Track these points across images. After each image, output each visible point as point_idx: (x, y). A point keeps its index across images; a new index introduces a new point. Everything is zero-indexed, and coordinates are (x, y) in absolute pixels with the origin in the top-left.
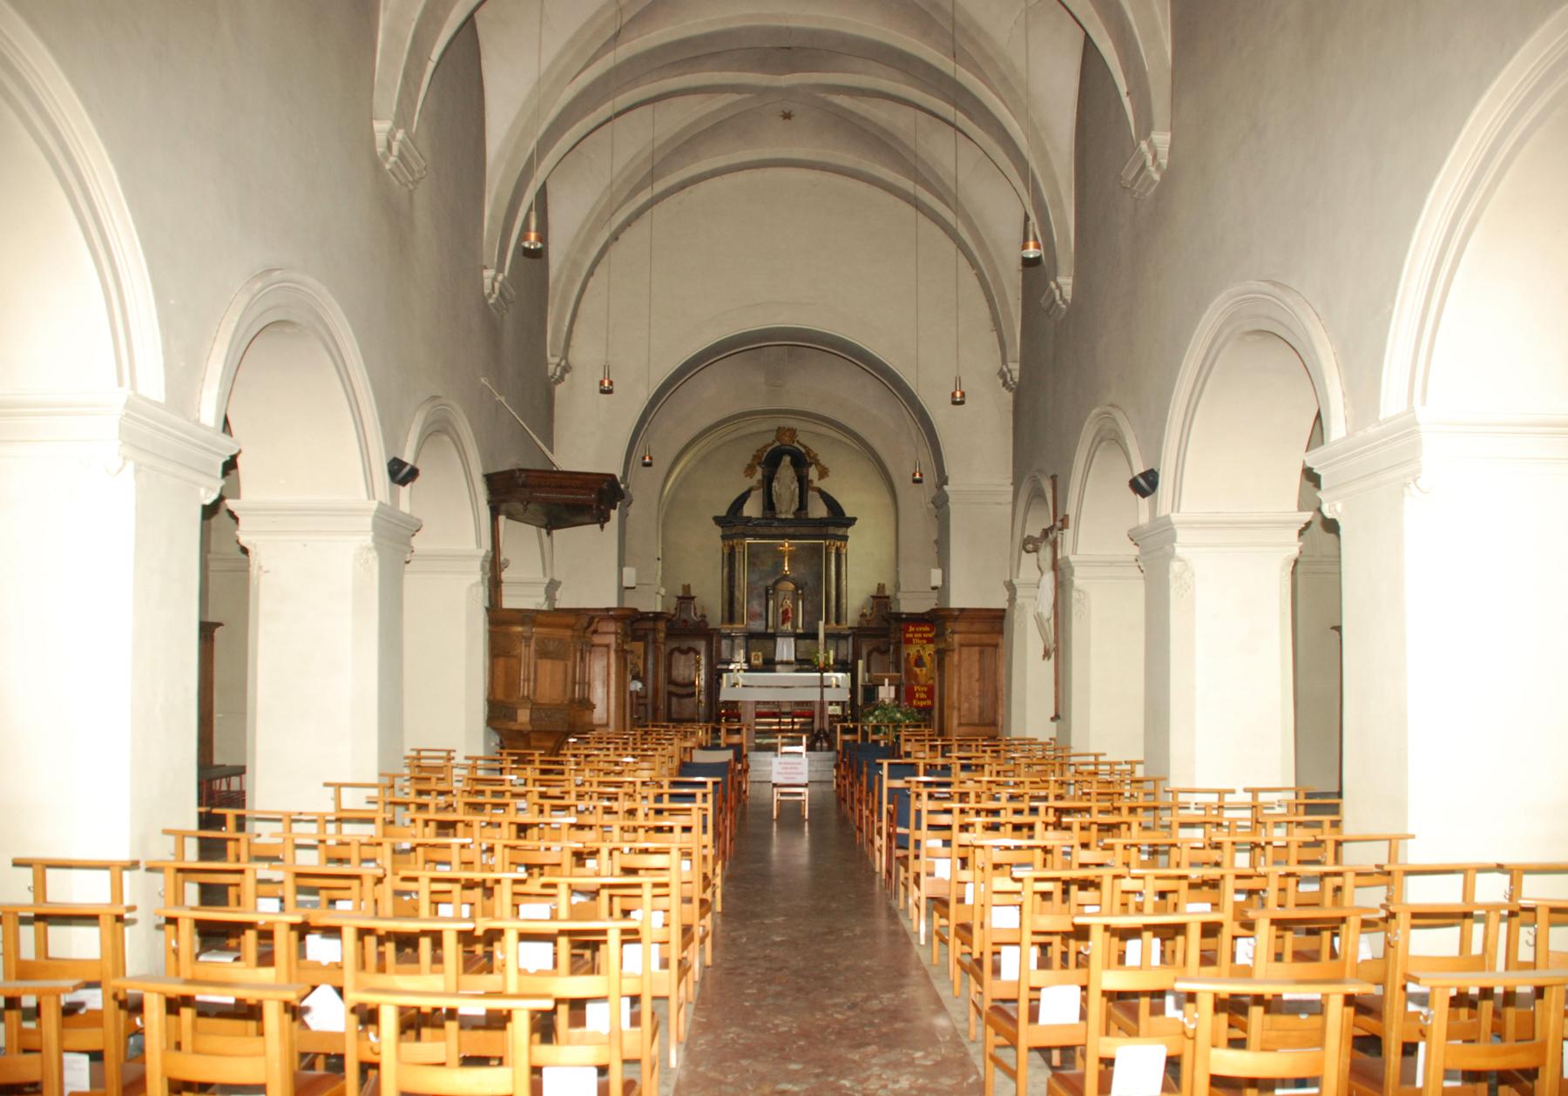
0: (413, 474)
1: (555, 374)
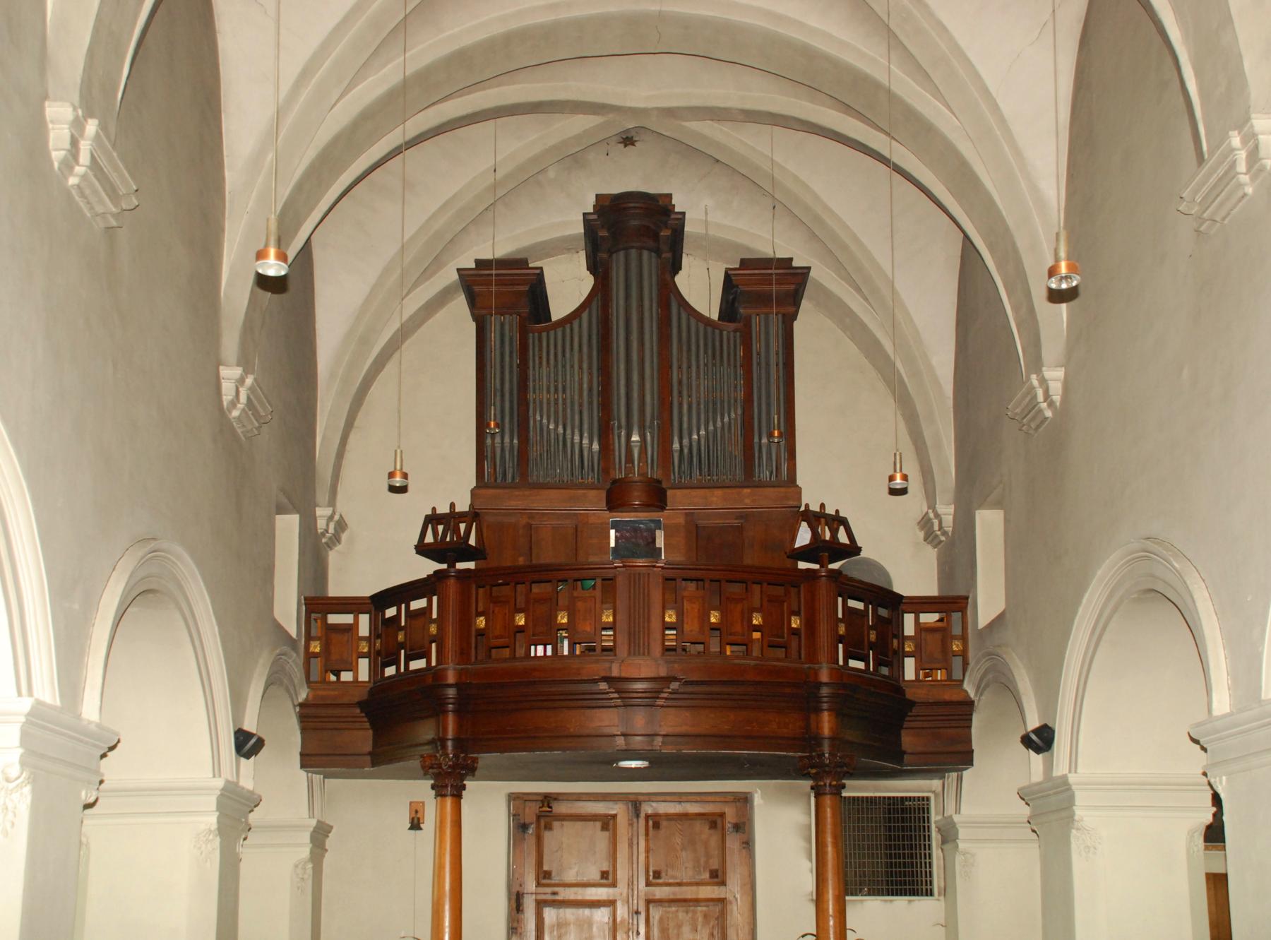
0: (260, 743)
1: (327, 531)
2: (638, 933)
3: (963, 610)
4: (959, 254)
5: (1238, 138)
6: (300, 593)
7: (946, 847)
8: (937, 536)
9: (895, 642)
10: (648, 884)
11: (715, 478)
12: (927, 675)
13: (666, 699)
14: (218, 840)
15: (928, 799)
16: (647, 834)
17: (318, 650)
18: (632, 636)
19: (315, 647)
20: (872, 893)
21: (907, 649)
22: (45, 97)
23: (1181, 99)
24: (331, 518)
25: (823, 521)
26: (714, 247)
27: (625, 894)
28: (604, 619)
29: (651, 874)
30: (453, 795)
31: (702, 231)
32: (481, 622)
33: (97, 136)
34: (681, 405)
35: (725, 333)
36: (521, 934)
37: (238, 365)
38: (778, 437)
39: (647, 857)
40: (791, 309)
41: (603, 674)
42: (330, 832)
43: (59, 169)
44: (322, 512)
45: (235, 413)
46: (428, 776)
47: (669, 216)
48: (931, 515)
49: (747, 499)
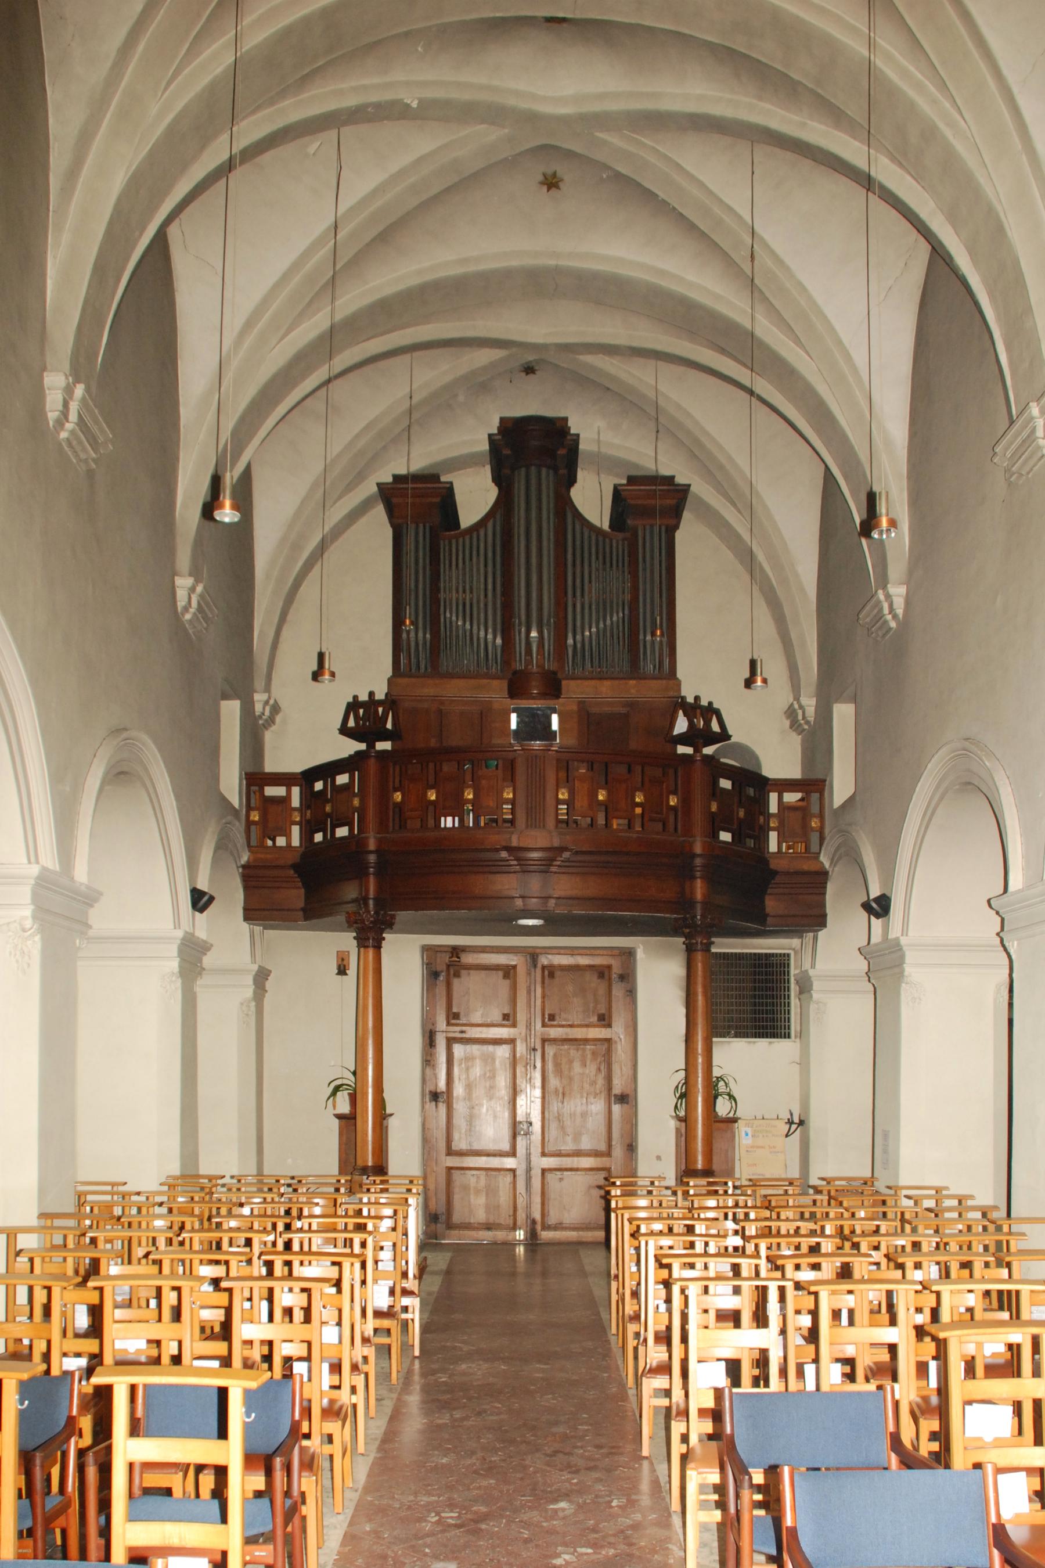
0: (212, 899)
1: (263, 714)
2: (535, 1067)
3: (822, 793)
5: (1037, 409)
6: (241, 768)
7: (802, 997)
8: (800, 725)
9: (762, 819)
10: (544, 1025)
11: (604, 669)
12: (788, 848)
13: (559, 866)
14: (179, 981)
15: (788, 955)
16: (543, 982)
17: (257, 818)
18: (529, 812)
19: (255, 816)
20: (737, 1035)
22: (44, 369)
23: (997, 368)
24: (267, 703)
25: (698, 711)
26: (604, 463)
27: (523, 1034)
28: (505, 796)
29: (547, 1016)
30: (374, 947)
31: (594, 448)
32: (398, 797)
33: (83, 399)
34: (574, 606)
35: (614, 542)
37: (190, 575)
39: (543, 1002)
40: (672, 522)
41: (504, 844)
42: (269, 976)
43: (54, 426)
44: (259, 698)
45: (188, 617)
46: (352, 929)
47: (565, 437)
48: (796, 706)
49: (633, 690)
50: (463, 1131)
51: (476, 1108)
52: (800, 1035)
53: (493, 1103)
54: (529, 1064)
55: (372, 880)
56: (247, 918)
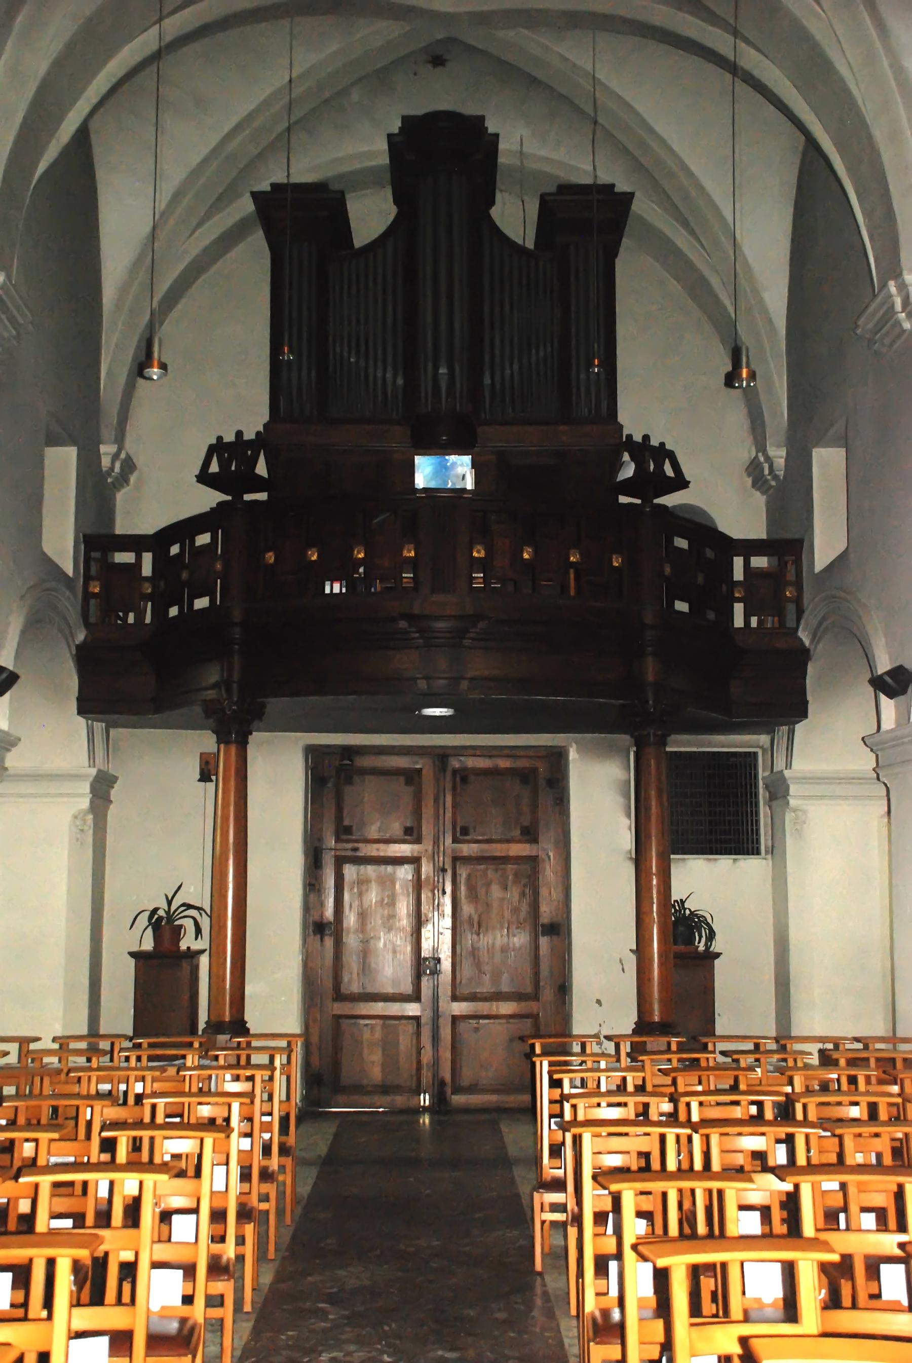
1: (112, 469)
2: (444, 893)
4: (795, 181)
7: (774, 803)
9: (724, 588)
10: (455, 840)
13: (473, 639)
15: (755, 754)
16: (454, 789)
17: (97, 590)
21: (737, 595)
24: (116, 457)
29: (458, 829)
30: (237, 742)
32: (270, 557)
36: (319, 891)
38: (598, 366)
39: (454, 814)
42: (115, 782)
44: (107, 450)
48: (762, 459)
50: (355, 971)
51: (372, 942)
52: (771, 851)
53: (391, 936)
54: (437, 889)
55: (236, 660)
56: (81, 712)
